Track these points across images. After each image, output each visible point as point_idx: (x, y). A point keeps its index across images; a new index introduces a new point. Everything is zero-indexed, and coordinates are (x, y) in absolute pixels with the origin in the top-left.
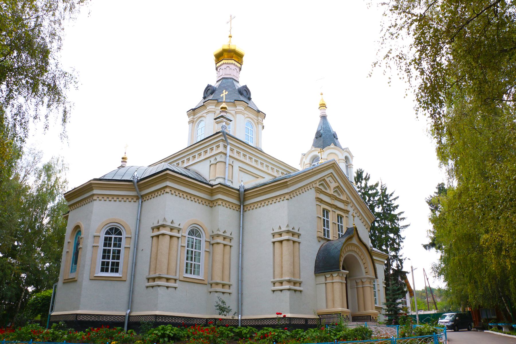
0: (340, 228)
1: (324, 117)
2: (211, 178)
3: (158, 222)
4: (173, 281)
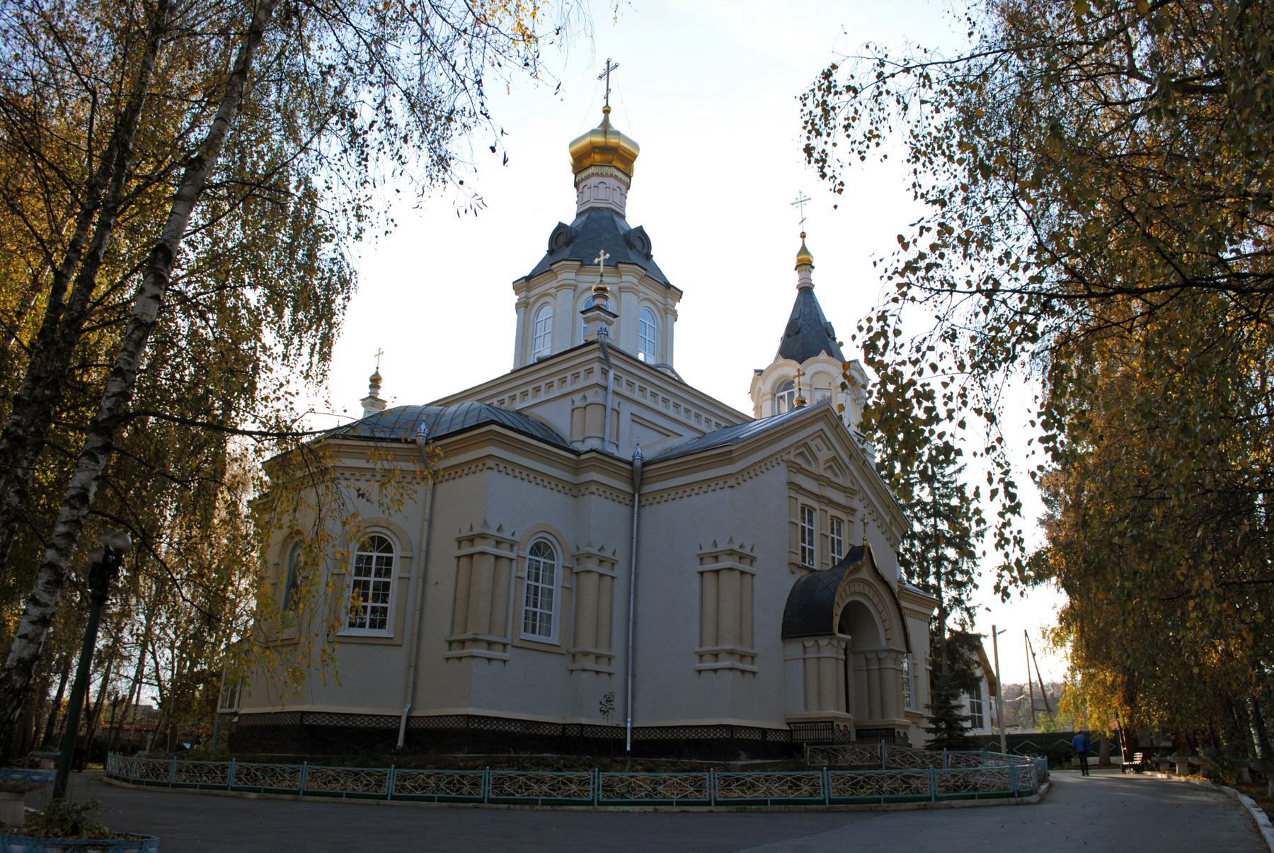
0: (836, 545)
1: (806, 292)
2: (575, 438)
3: (471, 529)
4: (501, 647)
